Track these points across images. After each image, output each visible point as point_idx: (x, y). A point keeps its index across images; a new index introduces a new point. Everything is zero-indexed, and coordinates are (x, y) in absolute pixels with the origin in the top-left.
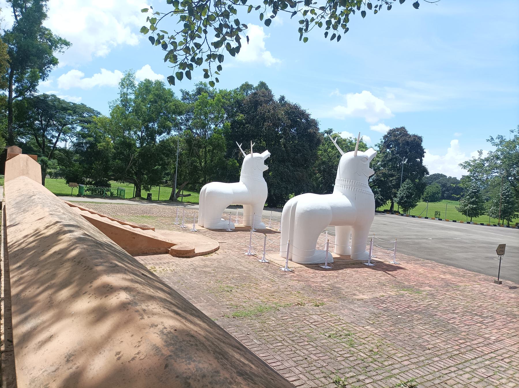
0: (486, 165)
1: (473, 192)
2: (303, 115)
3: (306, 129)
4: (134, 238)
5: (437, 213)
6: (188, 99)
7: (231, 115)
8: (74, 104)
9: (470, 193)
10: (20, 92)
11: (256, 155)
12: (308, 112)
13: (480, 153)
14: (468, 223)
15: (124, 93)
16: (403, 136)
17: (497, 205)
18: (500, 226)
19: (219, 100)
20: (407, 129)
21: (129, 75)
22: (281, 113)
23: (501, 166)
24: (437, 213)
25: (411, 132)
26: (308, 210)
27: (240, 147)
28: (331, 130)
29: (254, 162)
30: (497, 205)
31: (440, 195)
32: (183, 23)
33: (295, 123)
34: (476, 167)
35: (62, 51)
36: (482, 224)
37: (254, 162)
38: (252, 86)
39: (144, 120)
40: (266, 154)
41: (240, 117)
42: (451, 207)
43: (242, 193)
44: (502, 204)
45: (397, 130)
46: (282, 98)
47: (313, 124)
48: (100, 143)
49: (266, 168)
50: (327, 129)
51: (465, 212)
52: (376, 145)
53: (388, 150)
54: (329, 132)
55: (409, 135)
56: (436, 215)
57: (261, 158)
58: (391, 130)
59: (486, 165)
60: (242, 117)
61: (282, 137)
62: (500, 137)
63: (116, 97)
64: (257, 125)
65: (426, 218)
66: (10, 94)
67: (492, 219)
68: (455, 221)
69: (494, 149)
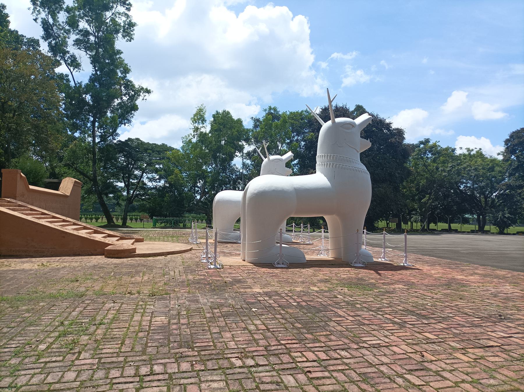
4: (64, 237)
10: (103, 138)
26: (256, 192)
32: (60, 12)
35: (145, 98)
50: (423, 139)
52: (499, 154)
60: (311, 135)
66: (94, 140)
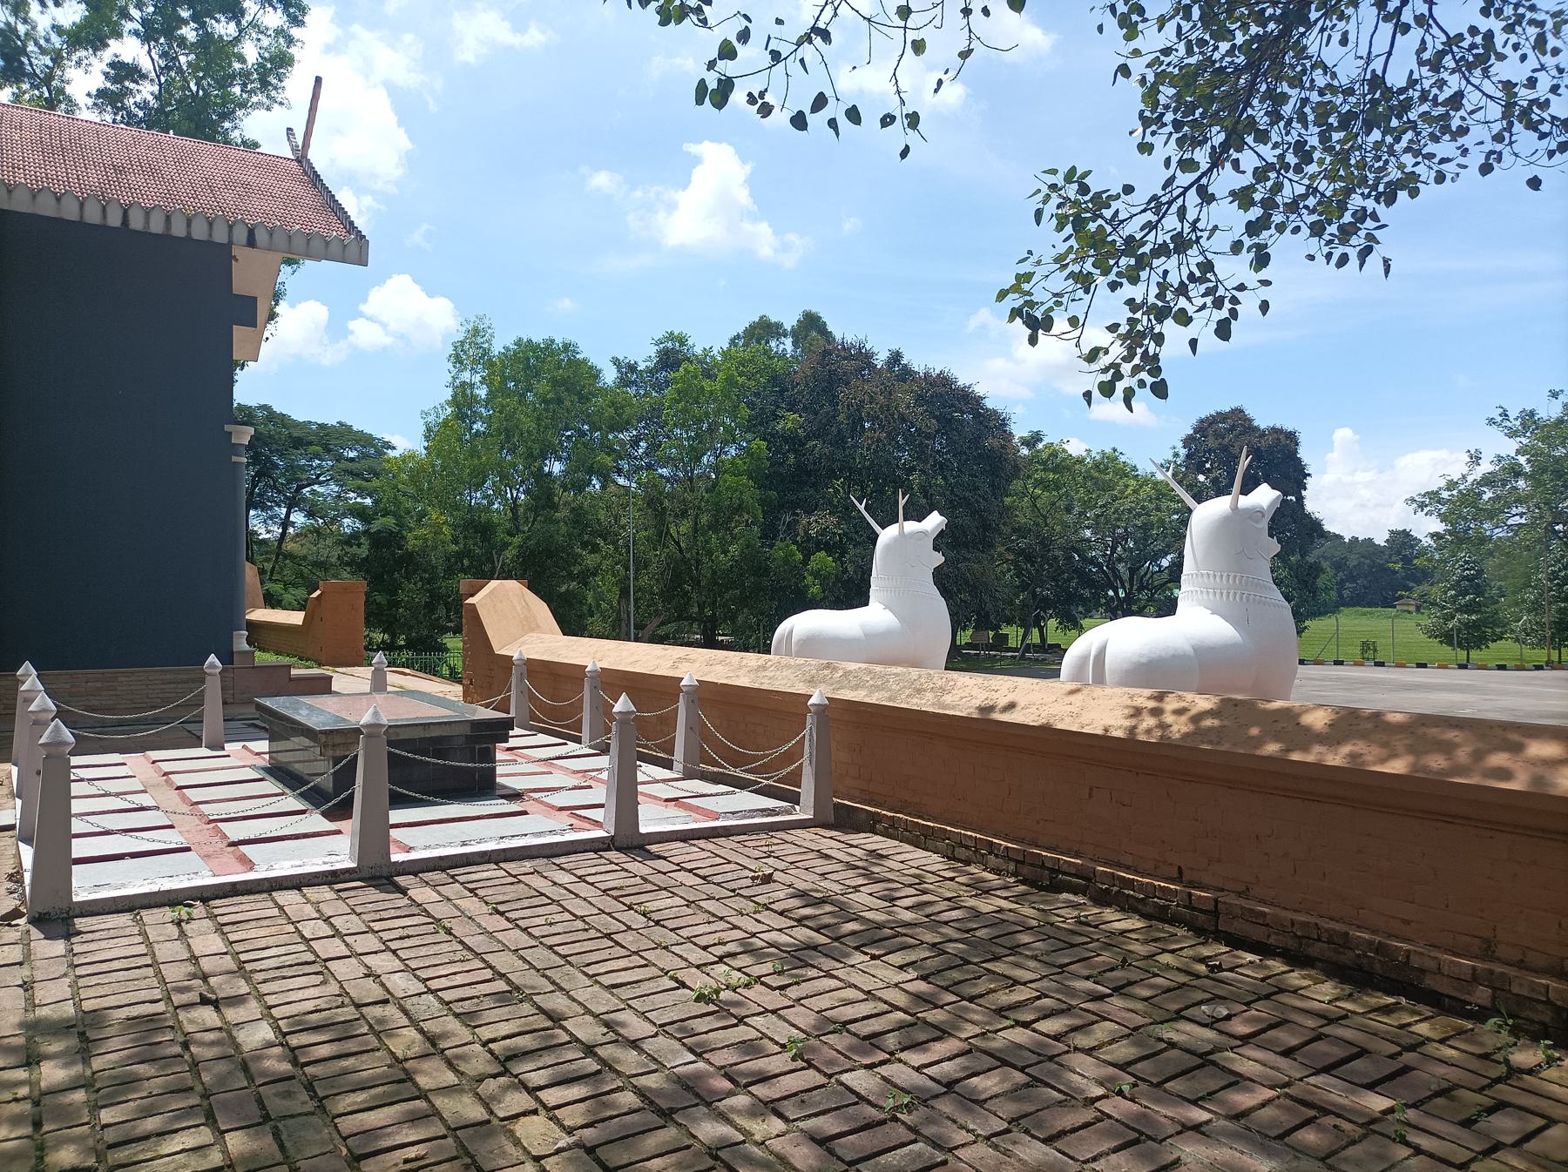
0: (1485, 497)
1: (1466, 578)
2: (968, 400)
3: (976, 440)
5: (1367, 647)
6: (634, 383)
7: (760, 423)
8: (322, 426)
9: (1458, 582)
11: (911, 526)
12: (979, 390)
13: (1475, 459)
14: (1462, 667)
15: (463, 384)
16: (1242, 433)
17: (1536, 607)
18: (1553, 668)
19: (730, 381)
20: (1250, 411)
21: (476, 332)
22: (904, 398)
23: (1529, 497)
24: (1367, 647)
25: (1262, 421)
26: (1144, 660)
27: (862, 508)
28: (1038, 433)
29: (906, 544)
30: (1536, 607)
31: (1333, 594)
33: (947, 424)
34: (1461, 505)
36: (1502, 667)
37: (906, 544)
38: (779, 325)
39: (530, 455)
40: (935, 521)
41: (790, 421)
42: (1405, 627)
43: (887, 634)
44: (1550, 603)
45: (1221, 417)
46: (896, 357)
47: (993, 423)
48: (411, 530)
49: (939, 559)
51: (1447, 638)
53: (1201, 478)
54: (1036, 438)
55: (1257, 428)
56: (1364, 651)
57: (924, 533)
58: (1202, 421)
59: (1488, 495)
61: (913, 469)
62: (1529, 417)
63: (436, 394)
64: (840, 441)
65: (1338, 663)
67: (1527, 651)
68: (1424, 666)
69: (1509, 447)
